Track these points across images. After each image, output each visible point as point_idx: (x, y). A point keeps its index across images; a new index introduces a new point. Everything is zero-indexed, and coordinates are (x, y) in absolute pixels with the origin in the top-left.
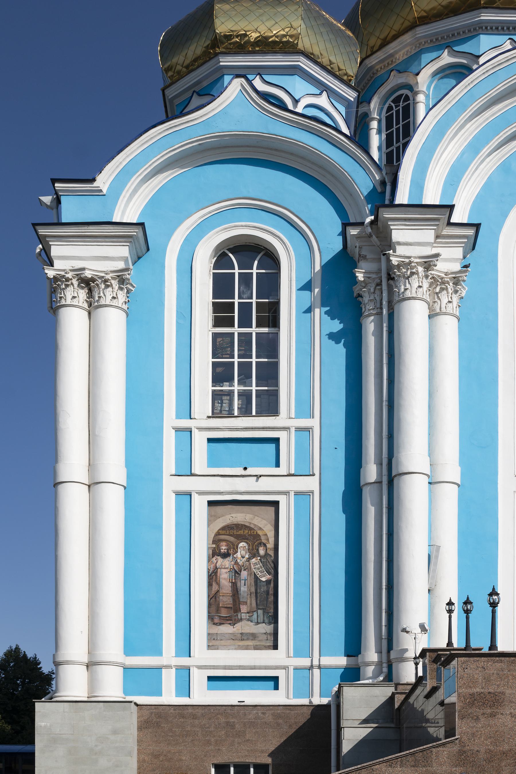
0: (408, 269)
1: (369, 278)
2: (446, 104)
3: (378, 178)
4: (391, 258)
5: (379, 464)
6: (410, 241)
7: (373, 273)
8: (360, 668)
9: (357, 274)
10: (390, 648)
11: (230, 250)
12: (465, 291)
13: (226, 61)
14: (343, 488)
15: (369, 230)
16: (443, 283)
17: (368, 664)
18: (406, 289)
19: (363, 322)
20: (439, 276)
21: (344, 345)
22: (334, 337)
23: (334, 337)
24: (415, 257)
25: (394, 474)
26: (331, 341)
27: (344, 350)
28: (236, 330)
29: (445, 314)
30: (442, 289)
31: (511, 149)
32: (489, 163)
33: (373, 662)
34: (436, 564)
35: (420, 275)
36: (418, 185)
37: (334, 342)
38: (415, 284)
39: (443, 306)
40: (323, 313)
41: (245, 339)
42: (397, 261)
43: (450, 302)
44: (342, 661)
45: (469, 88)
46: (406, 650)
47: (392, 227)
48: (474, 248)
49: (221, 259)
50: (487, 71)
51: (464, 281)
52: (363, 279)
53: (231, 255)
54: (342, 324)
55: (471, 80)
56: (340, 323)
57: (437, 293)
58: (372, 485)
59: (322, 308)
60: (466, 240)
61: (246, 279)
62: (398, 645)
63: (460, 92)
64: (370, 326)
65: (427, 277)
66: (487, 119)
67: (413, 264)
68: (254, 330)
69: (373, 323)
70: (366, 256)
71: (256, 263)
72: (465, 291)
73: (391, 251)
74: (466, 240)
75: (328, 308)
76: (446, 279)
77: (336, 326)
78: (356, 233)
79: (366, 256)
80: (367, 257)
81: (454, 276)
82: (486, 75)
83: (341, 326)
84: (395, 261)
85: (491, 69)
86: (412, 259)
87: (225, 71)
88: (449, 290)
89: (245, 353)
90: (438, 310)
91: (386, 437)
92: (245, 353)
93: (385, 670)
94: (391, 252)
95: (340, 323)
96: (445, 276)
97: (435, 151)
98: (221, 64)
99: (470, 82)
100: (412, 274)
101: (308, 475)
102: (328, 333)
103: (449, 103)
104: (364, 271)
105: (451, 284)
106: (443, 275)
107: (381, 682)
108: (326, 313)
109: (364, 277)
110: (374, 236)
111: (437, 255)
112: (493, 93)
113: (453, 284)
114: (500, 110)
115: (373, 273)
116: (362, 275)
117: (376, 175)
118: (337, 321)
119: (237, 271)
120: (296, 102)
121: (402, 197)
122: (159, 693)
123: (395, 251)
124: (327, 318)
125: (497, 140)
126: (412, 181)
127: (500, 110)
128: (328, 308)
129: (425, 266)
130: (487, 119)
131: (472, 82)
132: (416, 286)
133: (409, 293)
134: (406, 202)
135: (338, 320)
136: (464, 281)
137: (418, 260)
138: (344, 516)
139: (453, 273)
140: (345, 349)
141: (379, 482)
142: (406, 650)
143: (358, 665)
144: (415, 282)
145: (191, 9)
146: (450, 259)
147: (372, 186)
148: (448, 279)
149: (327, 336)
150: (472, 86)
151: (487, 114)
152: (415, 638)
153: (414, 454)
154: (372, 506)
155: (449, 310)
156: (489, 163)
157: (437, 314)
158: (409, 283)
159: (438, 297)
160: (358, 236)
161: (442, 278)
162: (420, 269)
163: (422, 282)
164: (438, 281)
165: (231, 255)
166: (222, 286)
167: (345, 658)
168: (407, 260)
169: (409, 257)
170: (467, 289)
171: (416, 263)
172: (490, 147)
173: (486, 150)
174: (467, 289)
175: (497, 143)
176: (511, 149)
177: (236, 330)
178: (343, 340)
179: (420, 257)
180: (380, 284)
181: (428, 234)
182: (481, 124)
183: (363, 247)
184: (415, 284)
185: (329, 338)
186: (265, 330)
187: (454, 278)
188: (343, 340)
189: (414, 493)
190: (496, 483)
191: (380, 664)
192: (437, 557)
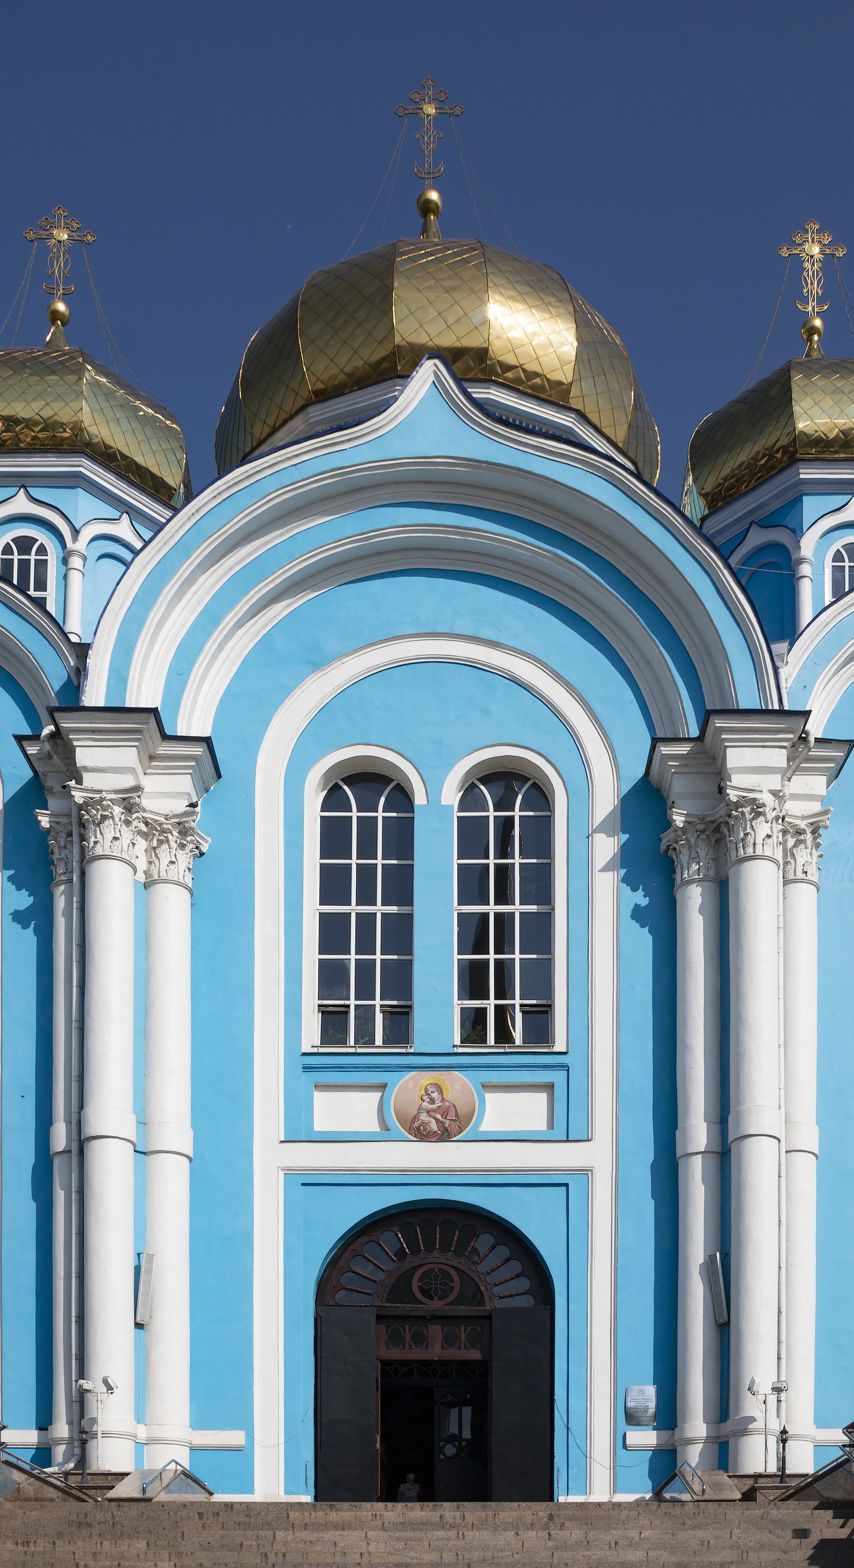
0: (98, 810)
1: (58, 823)
2: (160, 545)
3: (72, 664)
4: (73, 793)
5: (69, 1123)
6: (106, 765)
7: (63, 815)
8: (676, 1450)
9: (40, 818)
10: (82, 1416)
11: (346, 780)
12: (207, 845)
13: (807, 473)
14: (34, 1161)
15: (47, 747)
16: (163, 831)
17: (690, 1441)
18: (96, 843)
19: (679, 895)
20: (156, 821)
21: (35, 931)
22: (20, 917)
23: (20, 917)
24: (108, 792)
25: (731, 1138)
26: (15, 923)
27: (34, 939)
28: (353, 909)
29: (166, 881)
30: (160, 842)
31: (274, 617)
32: (241, 638)
33: (63, 1439)
34: (148, 1282)
35: (117, 819)
36: (119, 676)
37: (20, 926)
38: (109, 835)
39: (163, 867)
40: (5, 879)
41: (365, 921)
42: (737, 796)
43: (172, 862)
44: (31, 1437)
45: (194, 520)
46: (752, 1419)
47: (75, 743)
48: (837, 777)
49: (333, 798)
50: (219, 494)
51: (826, 827)
52: (48, 826)
53: (346, 788)
54: (32, 897)
55: (197, 508)
56: (29, 896)
57: (154, 848)
58: (62, 1155)
59: (4, 871)
60: (194, 764)
61: (368, 826)
62: (737, 1413)
63: (181, 527)
64: (694, 900)
65: (128, 823)
66: (231, 569)
67: (104, 803)
68: (379, 909)
69: (63, 897)
70: (52, 788)
71: (383, 800)
72: (207, 845)
73: (73, 782)
74: (194, 764)
75: (12, 872)
76: (165, 826)
77: (640, 898)
78: (35, 752)
79: (52, 788)
80: (54, 790)
81: (177, 820)
82: (219, 500)
83: (30, 900)
84: (79, 797)
85: (224, 490)
86: (104, 795)
87: (805, 488)
88: (172, 843)
89: (366, 946)
90: (156, 877)
91: (76, 1078)
92: (366, 946)
93: (77, 1451)
94: (72, 783)
95: (29, 896)
96: (165, 821)
97: (145, 621)
98: (802, 476)
99: (194, 511)
100: (104, 818)
101: (585, 1141)
102: (13, 911)
103: (165, 544)
104: (49, 812)
105: (175, 833)
106: (162, 819)
107: (72, 1469)
108: (10, 879)
109: (50, 822)
110: (55, 757)
111: (137, 789)
112: (231, 528)
113: (179, 833)
114: (249, 555)
115: (63, 815)
116: (47, 819)
117: (70, 659)
118: (24, 893)
119: (354, 814)
120: (76, 532)
121: (95, 694)
122: (251, 1491)
123: (79, 781)
124: (11, 887)
125: (246, 602)
126: (111, 669)
127: (249, 555)
128: (12, 872)
129: (124, 805)
130: (231, 569)
131: (197, 511)
132: (112, 837)
133: (101, 849)
134: (101, 704)
135: (27, 890)
136: (826, 827)
137: (113, 796)
138: (34, 1205)
139: (175, 816)
140: (35, 938)
141: (68, 1151)
142: (752, 1419)
143: (674, 1445)
144: (108, 830)
145: (749, 383)
146: (167, 792)
147: (65, 677)
148: (170, 827)
149: (11, 917)
150: (198, 516)
151: (229, 562)
152: (765, 1403)
153: (111, 1108)
154: (62, 1189)
155: (173, 876)
156: (241, 638)
157: (154, 882)
158: (101, 833)
159: (156, 854)
160: (40, 756)
161: (161, 824)
162: (117, 810)
163: (120, 831)
164: (156, 830)
165: (346, 788)
166: (334, 837)
167: (37, 1432)
168: (97, 796)
169: (100, 792)
170: (210, 841)
171: (111, 800)
172: (236, 614)
173: (230, 619)
174: (210, 841)
175: (247, 607)
176: (274, 617)
177: (353, 909)
178: (33, 923)
179: (116, 792)
180: (70, 834)
181: (126, 755)
182: (222, 577)
183: (49, 774)
184: (109, 835)
185: (14, 920)
186: (533, 908)
187: (179, 824)
188: (33, 923)
189: (111, 1170)
190: (251, 1154)
191: (709, 1440)
192: (149, 1271)
